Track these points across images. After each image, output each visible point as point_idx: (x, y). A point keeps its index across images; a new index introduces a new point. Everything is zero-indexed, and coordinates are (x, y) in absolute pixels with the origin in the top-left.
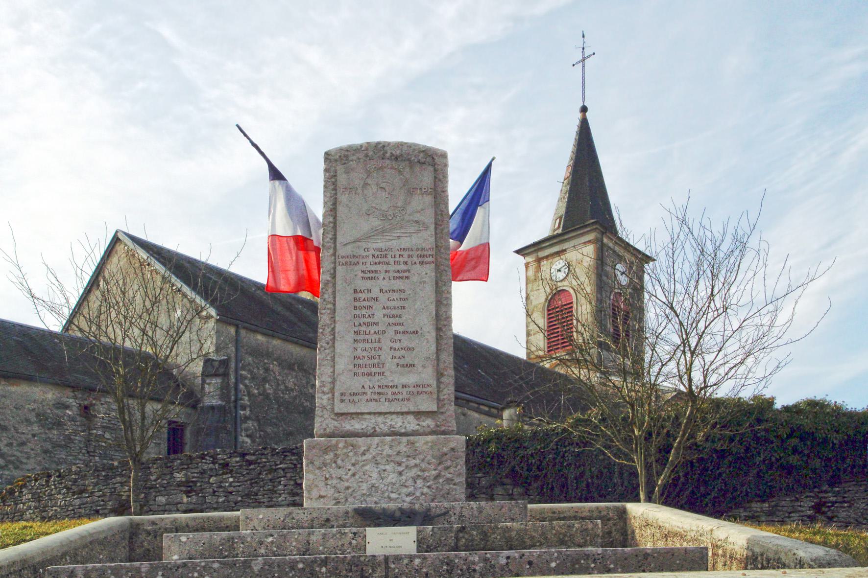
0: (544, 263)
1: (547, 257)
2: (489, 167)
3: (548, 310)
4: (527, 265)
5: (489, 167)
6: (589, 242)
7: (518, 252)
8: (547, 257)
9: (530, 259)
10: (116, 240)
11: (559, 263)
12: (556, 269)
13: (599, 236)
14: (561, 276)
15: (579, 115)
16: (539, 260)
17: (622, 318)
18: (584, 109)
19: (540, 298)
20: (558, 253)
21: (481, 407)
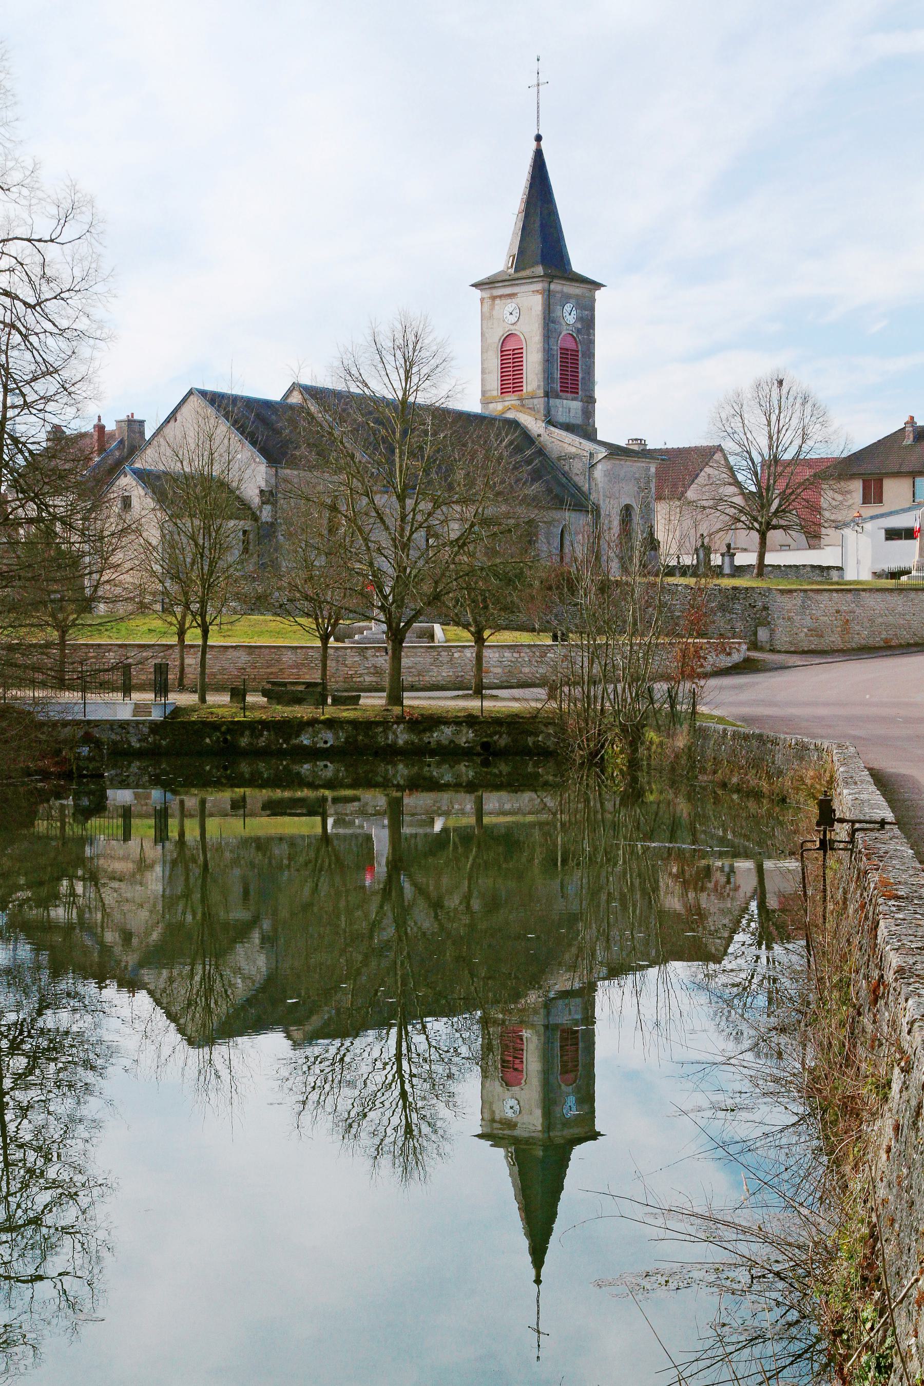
0: (498, 301)
1: (501, 297)
2: (538, 1254)
3: (502, 352)
4: (482, 300)
5: (538, 1254)
6: (537, 291)
7: (472, 286)
8: (501, 297)
9: (486, 294)
10: (190, 393)
11: (510, 306)
12: (506, 311)
13: (546, 285)
14: (513, 319)
15: (534, 144)
16: (494, 298)
17: (571, 368)
18: (539, 138)
19: (495, 338)
20: (512, 296)
21: (611, 920)
